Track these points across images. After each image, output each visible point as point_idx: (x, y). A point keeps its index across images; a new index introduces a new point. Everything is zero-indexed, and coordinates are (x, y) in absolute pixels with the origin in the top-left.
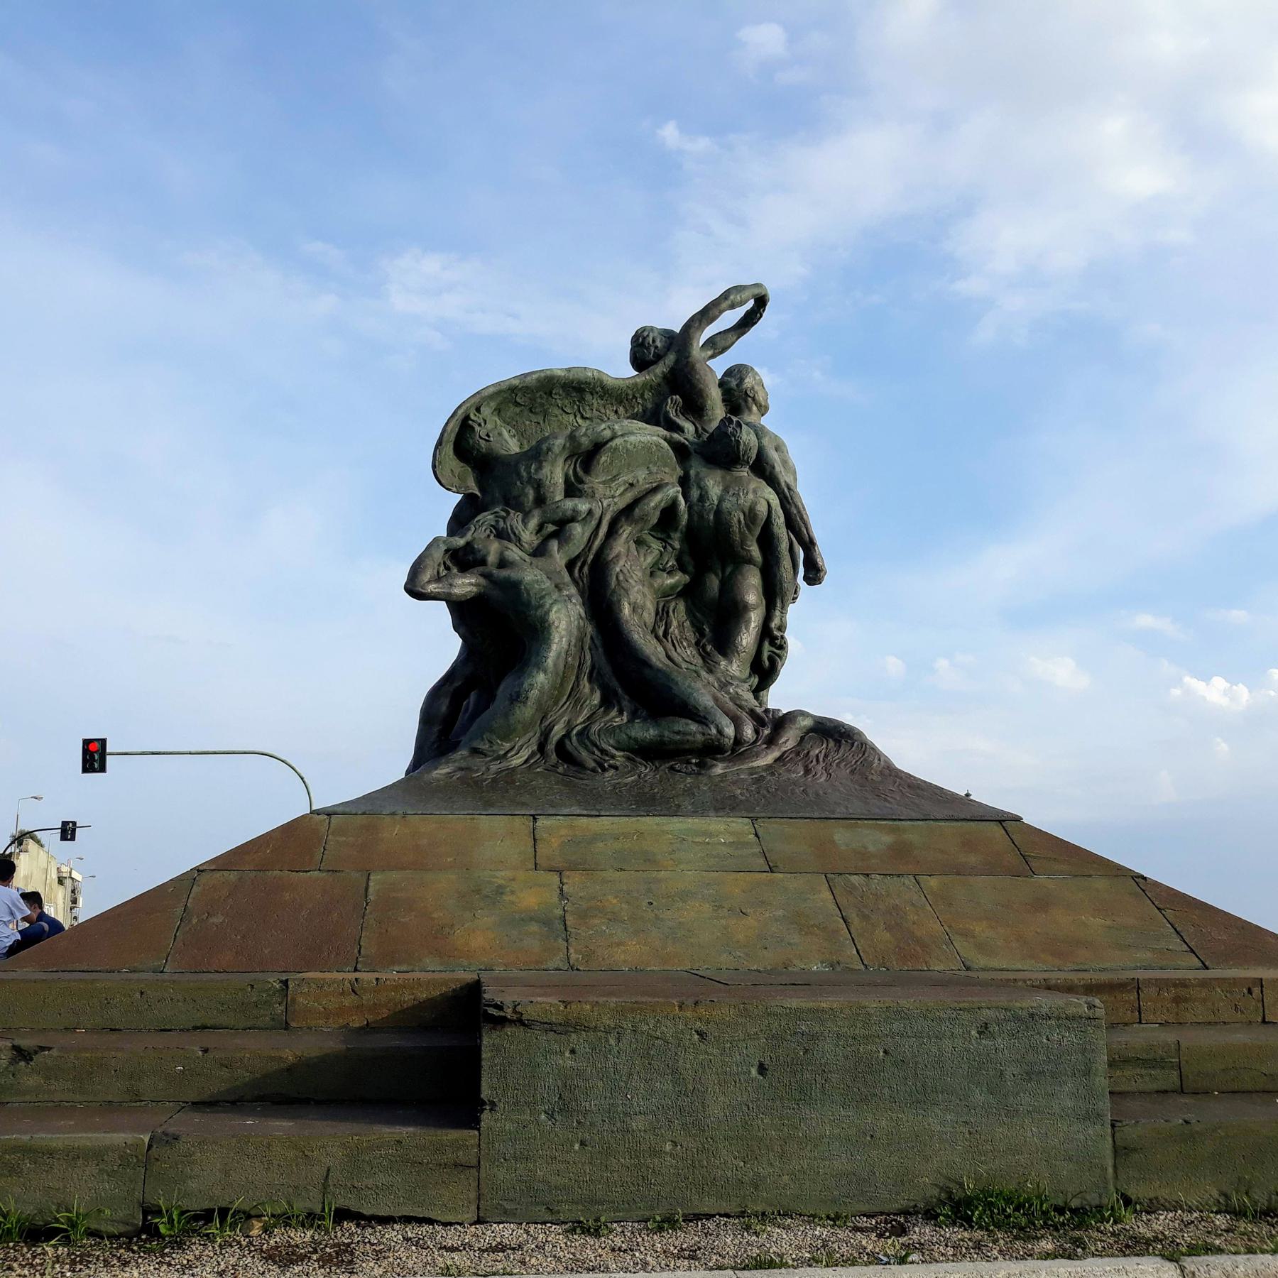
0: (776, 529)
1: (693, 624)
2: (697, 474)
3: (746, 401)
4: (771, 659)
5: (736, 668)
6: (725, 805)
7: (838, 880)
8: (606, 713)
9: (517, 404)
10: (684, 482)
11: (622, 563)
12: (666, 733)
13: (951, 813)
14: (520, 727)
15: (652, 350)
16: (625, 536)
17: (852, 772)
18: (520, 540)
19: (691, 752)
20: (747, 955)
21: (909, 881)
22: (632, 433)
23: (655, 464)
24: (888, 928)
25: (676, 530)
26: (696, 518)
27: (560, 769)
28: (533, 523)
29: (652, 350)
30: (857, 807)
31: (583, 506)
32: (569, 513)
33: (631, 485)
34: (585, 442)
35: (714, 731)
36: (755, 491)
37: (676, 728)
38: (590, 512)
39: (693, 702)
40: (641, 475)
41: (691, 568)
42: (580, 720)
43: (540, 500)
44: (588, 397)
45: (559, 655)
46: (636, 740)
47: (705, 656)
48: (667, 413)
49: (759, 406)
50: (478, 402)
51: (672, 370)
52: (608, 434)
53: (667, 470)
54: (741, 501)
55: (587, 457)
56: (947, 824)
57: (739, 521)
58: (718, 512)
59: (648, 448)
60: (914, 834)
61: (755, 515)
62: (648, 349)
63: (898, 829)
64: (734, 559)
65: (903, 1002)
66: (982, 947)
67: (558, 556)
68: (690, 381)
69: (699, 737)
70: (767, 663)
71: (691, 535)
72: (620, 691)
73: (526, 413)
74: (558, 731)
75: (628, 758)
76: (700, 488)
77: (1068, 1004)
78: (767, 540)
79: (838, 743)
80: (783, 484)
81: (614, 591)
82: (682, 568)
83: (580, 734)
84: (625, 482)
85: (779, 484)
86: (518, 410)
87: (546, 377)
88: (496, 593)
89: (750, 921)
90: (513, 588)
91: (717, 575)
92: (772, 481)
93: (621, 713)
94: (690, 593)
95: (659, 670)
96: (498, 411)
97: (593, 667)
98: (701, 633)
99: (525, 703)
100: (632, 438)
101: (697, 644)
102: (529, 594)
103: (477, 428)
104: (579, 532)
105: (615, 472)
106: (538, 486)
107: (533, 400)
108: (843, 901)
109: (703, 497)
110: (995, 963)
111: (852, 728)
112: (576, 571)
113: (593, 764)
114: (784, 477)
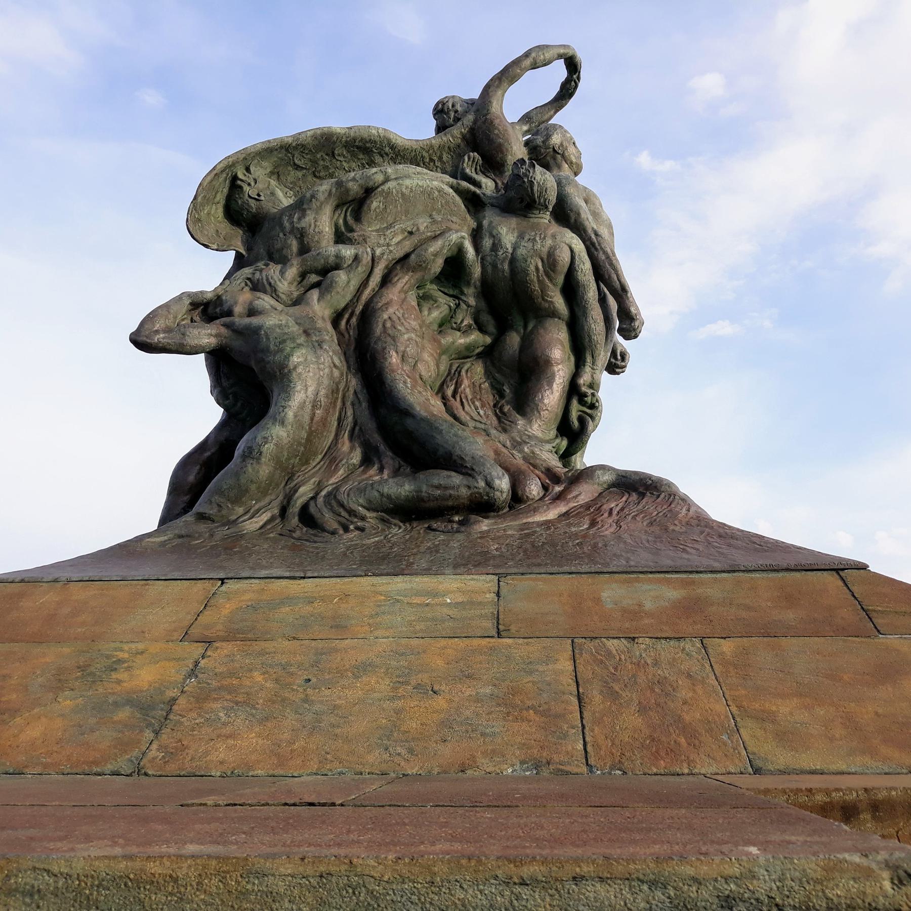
0: (580, 277)
1: (492, 386)
2: (491, 222)
3: (555, 159)
4: (582, 420)
5: (539, 430)
6: (474, 561)
7: (590, 645)
8: (364, 472)
9: (297, 167)
10: (476, 236)
11: (391, 310)
12: (424, 488)
13: (768, 562)
14: (253, 487)
15: (452, 114)
16: (400, 285)
17: (651, 524)
18: (275, 290)
19: (456, 509)
20: (411, 751)
21: (692, 646)
22: (408, 177)
23: (439, 212)
24: (643, 709)
25: (468, 284)
26: (489, 269)
27: (297, 534)
28: (292, 272)
29: (452, 114)
30: (643, 558)
31: (348, 252)
32: (332, 260)
33: (411, 233)
34: (354, 188)
35: (482, 484)
36: (554, 237)
37: (436, 482)
38: (356, 258)
39: (458, 452)
40: (423, 223)
41: (491, 328)
42: (333, 480)
43: (304, 250)
44: (378, 159)
45: (302, 406)
46: (389, 497)
47: (501, 416)
48: (463, 169)
49: (571, 164)
50: (247, 159)
51: (472, 130)
52: (380, 178)
53: (454, 219)
54: (538, 246)
55: (355, 205)
56: (765, 575)
57: (537, 269)
58: (513, 260)
59: (427, 193)
60: (712, 588)
61: (555, 260)
62: (447, 113)
63: (693, 582)
64: (533, 311)
65: (367, 862)
66: (786, 737)
67: (320, 308)
68: (490, 141)
69: (464, 492)
70: (576, 424)
71: (487, 290)
72: (382, 447)
73: (310, 178)
74: (304, 492)
75: (383, 520)
76: (492, 236)
77: (833, 869)
78: (571, 289)
79: (642, 495)
80: (590, 231)
81: (379, 339)
82: (481, 329)
83: (329, 494)
84: (403, 231)
85: (585, 231)
86: (300, 174)
87: (322, 135)
88: (237, 343)
89: (440, 702)
90: (251, 334)
91: (517, 331)
92: (578, 229)
93: (381, 470)
94: (489, 354)
95: (423, 420)
96: (276, 173)
97: (355, 423)
98: (501, 394)
99: (258, 459)
100: (408, 182)
101: (495, 406)
102: (268, 339)
103: (246, 188)
104: (345, 283)
105: (390, 219)
106: (301, 235)
107: (314, 162)
108: (585, 672)
109: (496, 246)
110: (807, 761)
111: (660, 480)
112: (343, 323)
113: (335, 526)
114: (590, 223)
